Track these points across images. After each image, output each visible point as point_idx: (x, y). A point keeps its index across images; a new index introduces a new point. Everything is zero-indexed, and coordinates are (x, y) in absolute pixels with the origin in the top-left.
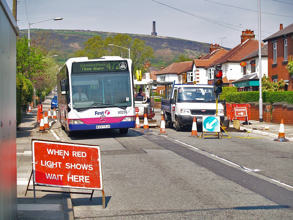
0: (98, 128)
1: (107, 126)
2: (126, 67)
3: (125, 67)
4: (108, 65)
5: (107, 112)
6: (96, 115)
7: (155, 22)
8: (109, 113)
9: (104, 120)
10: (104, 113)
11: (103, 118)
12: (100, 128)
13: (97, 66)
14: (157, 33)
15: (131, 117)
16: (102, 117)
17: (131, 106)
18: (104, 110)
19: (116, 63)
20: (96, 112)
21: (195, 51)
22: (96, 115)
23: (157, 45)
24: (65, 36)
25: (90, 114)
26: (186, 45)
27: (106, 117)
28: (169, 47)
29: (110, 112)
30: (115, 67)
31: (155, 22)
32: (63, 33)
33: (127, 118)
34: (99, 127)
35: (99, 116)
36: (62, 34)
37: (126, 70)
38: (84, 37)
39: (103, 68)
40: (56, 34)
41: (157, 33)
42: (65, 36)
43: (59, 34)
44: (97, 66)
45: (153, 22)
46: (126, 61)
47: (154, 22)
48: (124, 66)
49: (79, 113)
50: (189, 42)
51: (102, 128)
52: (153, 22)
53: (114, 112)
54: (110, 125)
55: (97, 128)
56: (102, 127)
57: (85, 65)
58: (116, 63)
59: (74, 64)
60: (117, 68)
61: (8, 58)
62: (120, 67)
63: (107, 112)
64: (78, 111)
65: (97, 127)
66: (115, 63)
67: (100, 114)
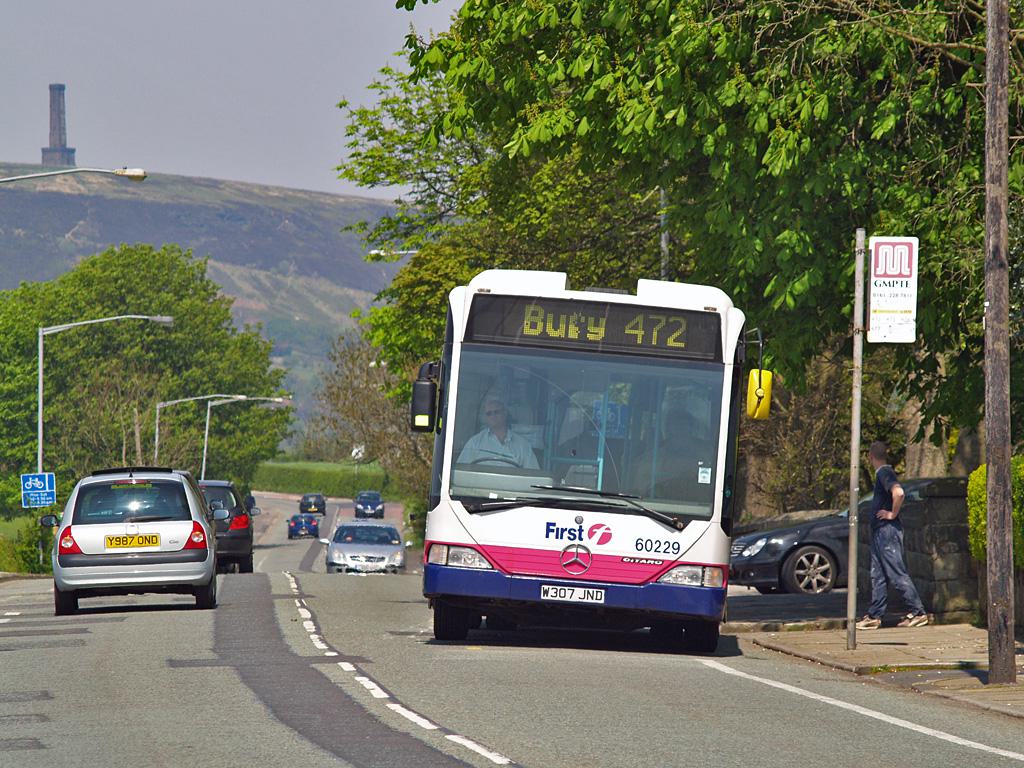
0: (549, 598)
4: (632, 324)
5: (599, 533)
6: (547, 536)
7: (61, 88)
8: (605, 539)
9: (580, 565)
10: (585, 535)
11: (578, 555)
12: (558, 598)
14: (73, 151)
16: (573, 550)
18: (590, 518)
19: (671, 320)
20: (551, 527)
21: (240, 270)
22: (547, 536)
25: (522, 529)
26: (204, 229)
27: (593, 552)
31: (61, 88)
34: (551, 594)
41: (73, 151)
45: (52, 88)
47: (57, 91)
50: (222, 216)
51: (567, 599)
52: (52, 88)
53: (628, 536)
54: (603, 591)
55: (542, 597)
56: (569, 593)
58: (671, 320)
63: (599, 533)
64: (471, 512)
65: (546, 592)
67: (566, 534)
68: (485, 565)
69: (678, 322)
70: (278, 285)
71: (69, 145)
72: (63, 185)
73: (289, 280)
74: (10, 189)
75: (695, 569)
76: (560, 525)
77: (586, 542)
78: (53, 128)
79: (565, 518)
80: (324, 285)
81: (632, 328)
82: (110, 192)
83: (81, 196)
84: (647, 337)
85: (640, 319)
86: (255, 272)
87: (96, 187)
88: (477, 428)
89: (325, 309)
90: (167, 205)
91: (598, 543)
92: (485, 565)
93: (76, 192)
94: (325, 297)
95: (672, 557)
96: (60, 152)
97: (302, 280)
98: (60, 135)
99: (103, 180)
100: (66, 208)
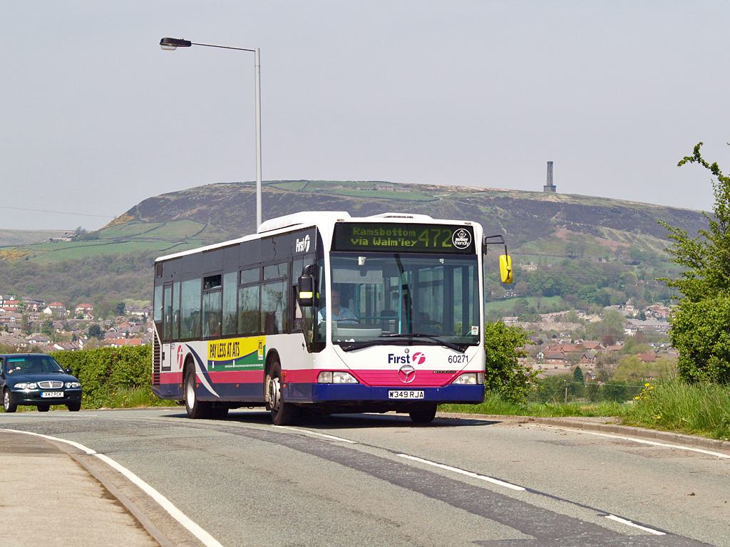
0: (394, 397)
1: (416, 393)
2: (468, 241)
3: (466, 243)
4: (422, 235)
7: (552, 163)
8: (422, 360)
10: (410, 360)
13: (395, 235)
14: (555, 187)
15: (476, 373)
17: (478, 345)
18: (414, 349)
19: (444, 231)
20: (391, 357)
21: (619, 232)
23: (541, 220)
24: (354, 204)
25: (375, 359)
28: (564, 223)
29: (424, 358)
30: (440, 240)
31: (552, 163)
32: (351, 196)
33: (465, 377)
35: (396, 367)
36: (349, 198)
37: (470, 251)
38: (390, 205)
39: (414, 243)
40: (338, 199)
41: (555, 187)
42: (355, 201)
43: (343, 199)
44: (395, 235)
45: (548, 163)
46: (471, 229)
47: (550, 164)
48: (464, 240)
49: (349, 353)
50: (612, 211)
51: (409, 397)
52: (548, 163)
53: (437, 358)
54: (423, 392)
57: (365, 231)
58: (444, 231)
59: (340, 228)
60: (444, 244)
61: (693, 494)
62: (454, 240)
65: (392, 394)
66: (439, 231)
67: (400, 360)
70: (634, 238)
71: (554, 184)
72: (552, 199)
73: (638, 236)
76: (396, 355)
78: (548, 178)
79: (399, 351)
80: (652, 238)
81: (422, 238)
82: (569, 201)
84: (431, 243)
85: (426, 232)
86: (625, 233)
87: (564, 200)
89: (652, 247)
90: (592, 207)
91: (419, 363)
94: (652, 242)
96: (551, 187)
97: (643, 236)
99: (567, 197)
100: (554, 207)
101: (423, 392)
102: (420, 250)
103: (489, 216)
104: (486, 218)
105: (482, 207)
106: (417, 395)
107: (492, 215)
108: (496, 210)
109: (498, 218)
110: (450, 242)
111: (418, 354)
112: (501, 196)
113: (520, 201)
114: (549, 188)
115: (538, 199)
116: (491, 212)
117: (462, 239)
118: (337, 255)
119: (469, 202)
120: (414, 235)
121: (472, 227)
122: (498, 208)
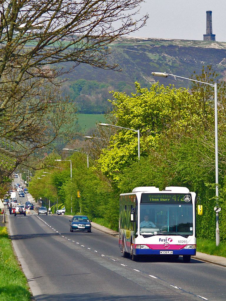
0: (162, 254)
2: (190, 199)
4: (173, 197)
5: (170, 240)
7: (211, 12)
8: (171, 241)
10: (167, 240)
12: (165, 254)
14: (215, 35)
17: (192, 235)
18: (169, 237)
25: (155, 240)
31: (211, 12)
35: (162, 243)
41: (215, 35)
44: (164, 197)
45: (207, 12)
46: (190, 195)
47: (209, 13)
52: (207, 12)
54: (172, 251)
59: (144, 195)
60: (181, 200)
62: (185, 199)
63: (170, 240)
64: (145, 237)
65: (161, 253)
67: (163, 241)
68: (148, 248)
69: (182, 196)
72: (213, 46)
74: (197, 48)
75: (191, 246)
76: (162, 239)
77: (168, 241)
78: (207, 27)
83: (222, 49)
84: (177, 200)
88: (144, 220)
92: (148, 248)
93: (221, 48)
95: (185, 244)
96: (210, 36)
98: (210, 29)
101: (172, 251)
102: (172, 202)
103: (157, 63)
104: (155, 65)
105: (151, 54)
106: (170, 253)
107: (161, 62)
108: (164, 57)
109: (166, 64)
110: (183, 199)
111: (170, 238)
112: (166, 44)
113: (184, 48)
114: (209, 37)
115: (201, 46)
116: (160, 59)
117: (187, 198)
118: (142, 205)
119: (137, 50)
120: (171, 197)
121: (191, 194)
122: (166, 55)
